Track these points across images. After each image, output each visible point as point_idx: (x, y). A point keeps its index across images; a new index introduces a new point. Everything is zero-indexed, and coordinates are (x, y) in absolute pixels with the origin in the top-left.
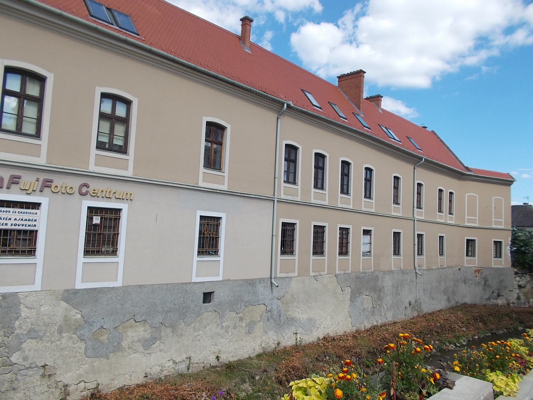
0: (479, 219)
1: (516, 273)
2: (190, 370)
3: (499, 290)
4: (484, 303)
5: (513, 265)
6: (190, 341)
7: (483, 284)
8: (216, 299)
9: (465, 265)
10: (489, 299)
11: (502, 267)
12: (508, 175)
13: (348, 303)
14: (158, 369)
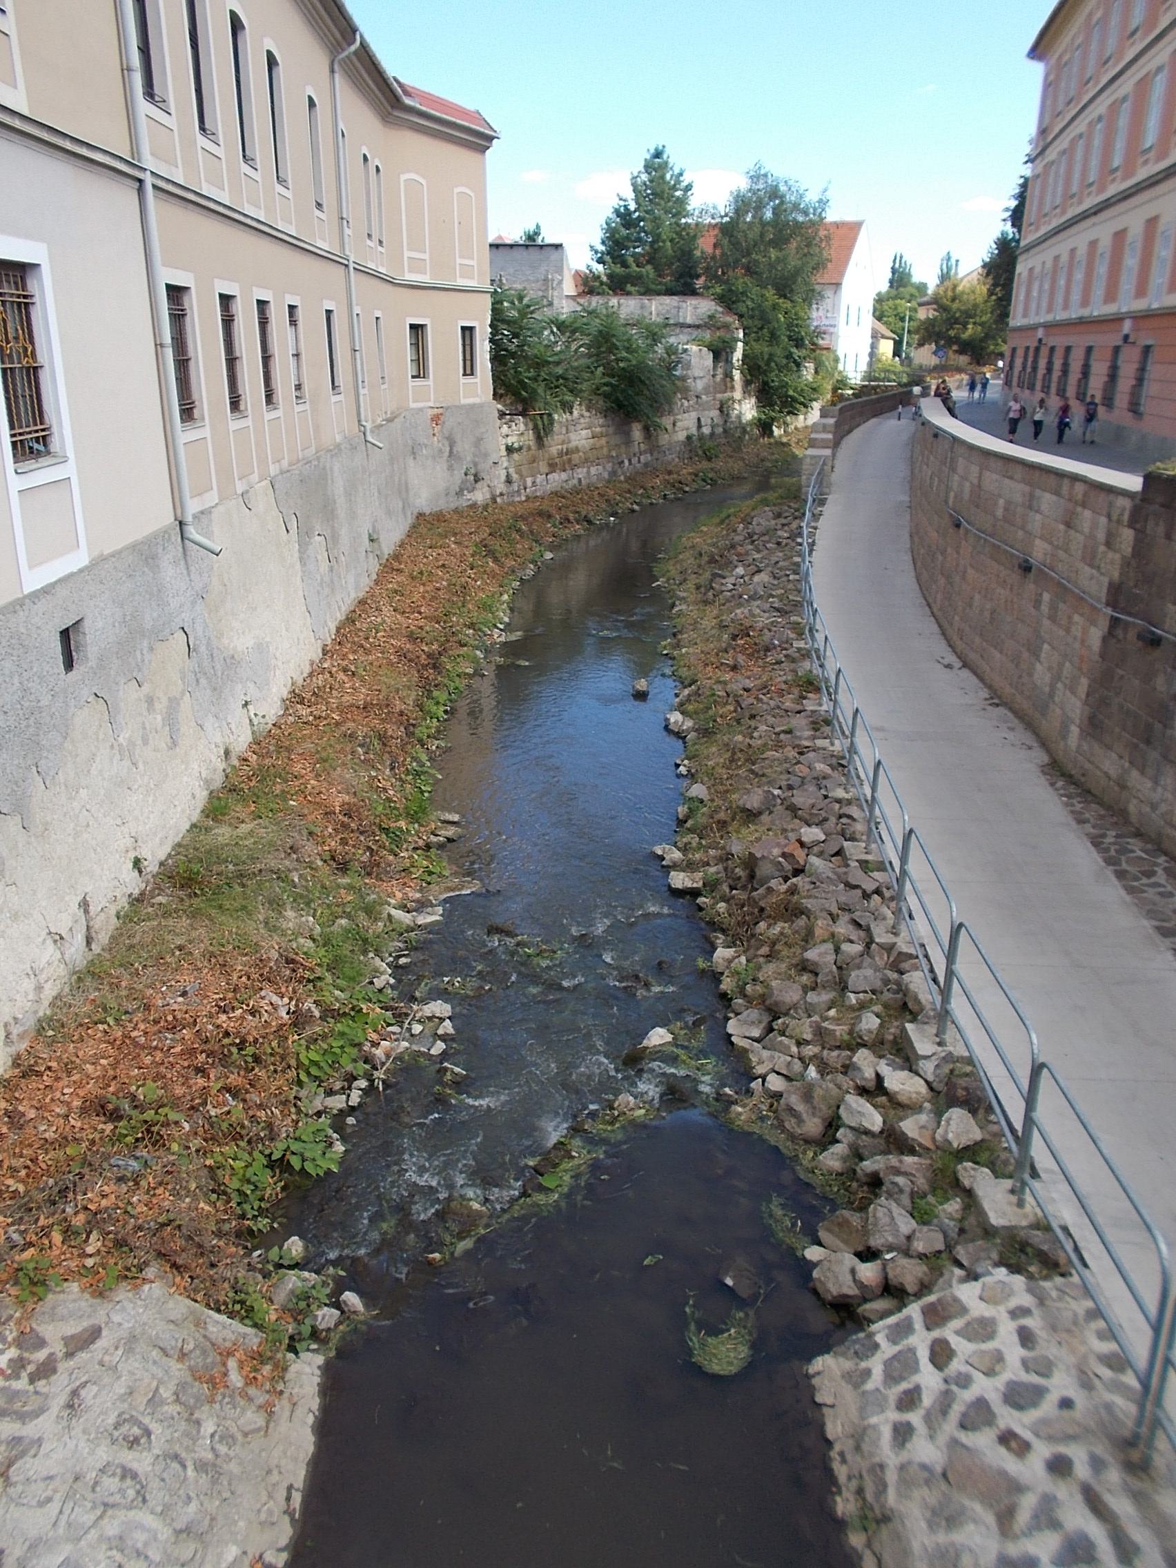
0: (431, 258)
1: (502, 415)
2: (93, 946)
3: (476, 464)
4: (453, 506)
5: (496, 396)
6: (71, 840)
7: (447, 454)
8: (93, 643)
9: (413, 405)
10: (460, 493)
11: (477, 400)
12: (477, 116)
13: (298, 566)
14: (28, 985)
